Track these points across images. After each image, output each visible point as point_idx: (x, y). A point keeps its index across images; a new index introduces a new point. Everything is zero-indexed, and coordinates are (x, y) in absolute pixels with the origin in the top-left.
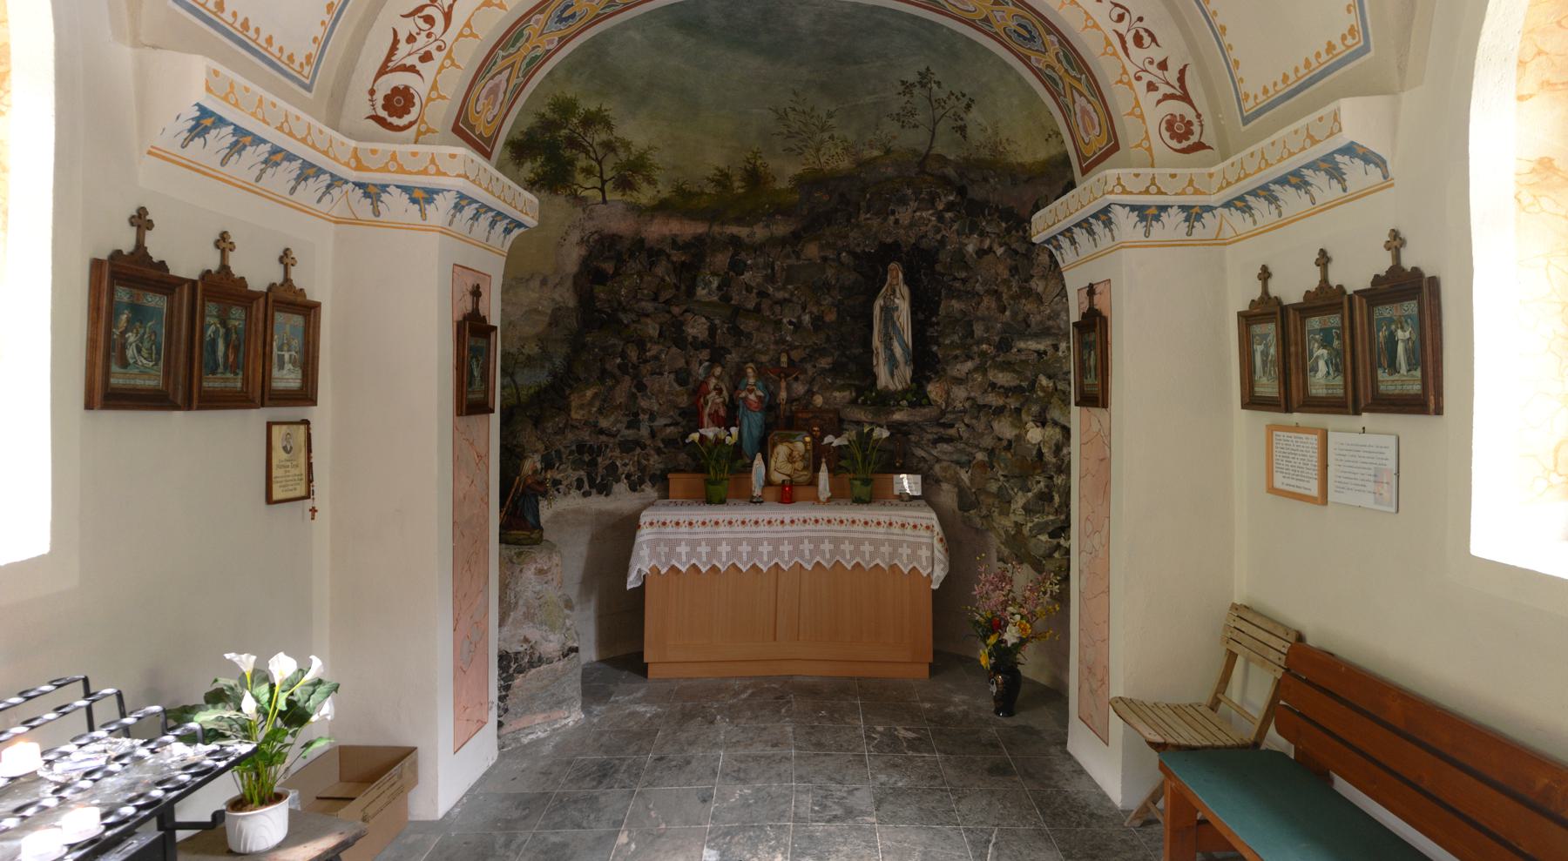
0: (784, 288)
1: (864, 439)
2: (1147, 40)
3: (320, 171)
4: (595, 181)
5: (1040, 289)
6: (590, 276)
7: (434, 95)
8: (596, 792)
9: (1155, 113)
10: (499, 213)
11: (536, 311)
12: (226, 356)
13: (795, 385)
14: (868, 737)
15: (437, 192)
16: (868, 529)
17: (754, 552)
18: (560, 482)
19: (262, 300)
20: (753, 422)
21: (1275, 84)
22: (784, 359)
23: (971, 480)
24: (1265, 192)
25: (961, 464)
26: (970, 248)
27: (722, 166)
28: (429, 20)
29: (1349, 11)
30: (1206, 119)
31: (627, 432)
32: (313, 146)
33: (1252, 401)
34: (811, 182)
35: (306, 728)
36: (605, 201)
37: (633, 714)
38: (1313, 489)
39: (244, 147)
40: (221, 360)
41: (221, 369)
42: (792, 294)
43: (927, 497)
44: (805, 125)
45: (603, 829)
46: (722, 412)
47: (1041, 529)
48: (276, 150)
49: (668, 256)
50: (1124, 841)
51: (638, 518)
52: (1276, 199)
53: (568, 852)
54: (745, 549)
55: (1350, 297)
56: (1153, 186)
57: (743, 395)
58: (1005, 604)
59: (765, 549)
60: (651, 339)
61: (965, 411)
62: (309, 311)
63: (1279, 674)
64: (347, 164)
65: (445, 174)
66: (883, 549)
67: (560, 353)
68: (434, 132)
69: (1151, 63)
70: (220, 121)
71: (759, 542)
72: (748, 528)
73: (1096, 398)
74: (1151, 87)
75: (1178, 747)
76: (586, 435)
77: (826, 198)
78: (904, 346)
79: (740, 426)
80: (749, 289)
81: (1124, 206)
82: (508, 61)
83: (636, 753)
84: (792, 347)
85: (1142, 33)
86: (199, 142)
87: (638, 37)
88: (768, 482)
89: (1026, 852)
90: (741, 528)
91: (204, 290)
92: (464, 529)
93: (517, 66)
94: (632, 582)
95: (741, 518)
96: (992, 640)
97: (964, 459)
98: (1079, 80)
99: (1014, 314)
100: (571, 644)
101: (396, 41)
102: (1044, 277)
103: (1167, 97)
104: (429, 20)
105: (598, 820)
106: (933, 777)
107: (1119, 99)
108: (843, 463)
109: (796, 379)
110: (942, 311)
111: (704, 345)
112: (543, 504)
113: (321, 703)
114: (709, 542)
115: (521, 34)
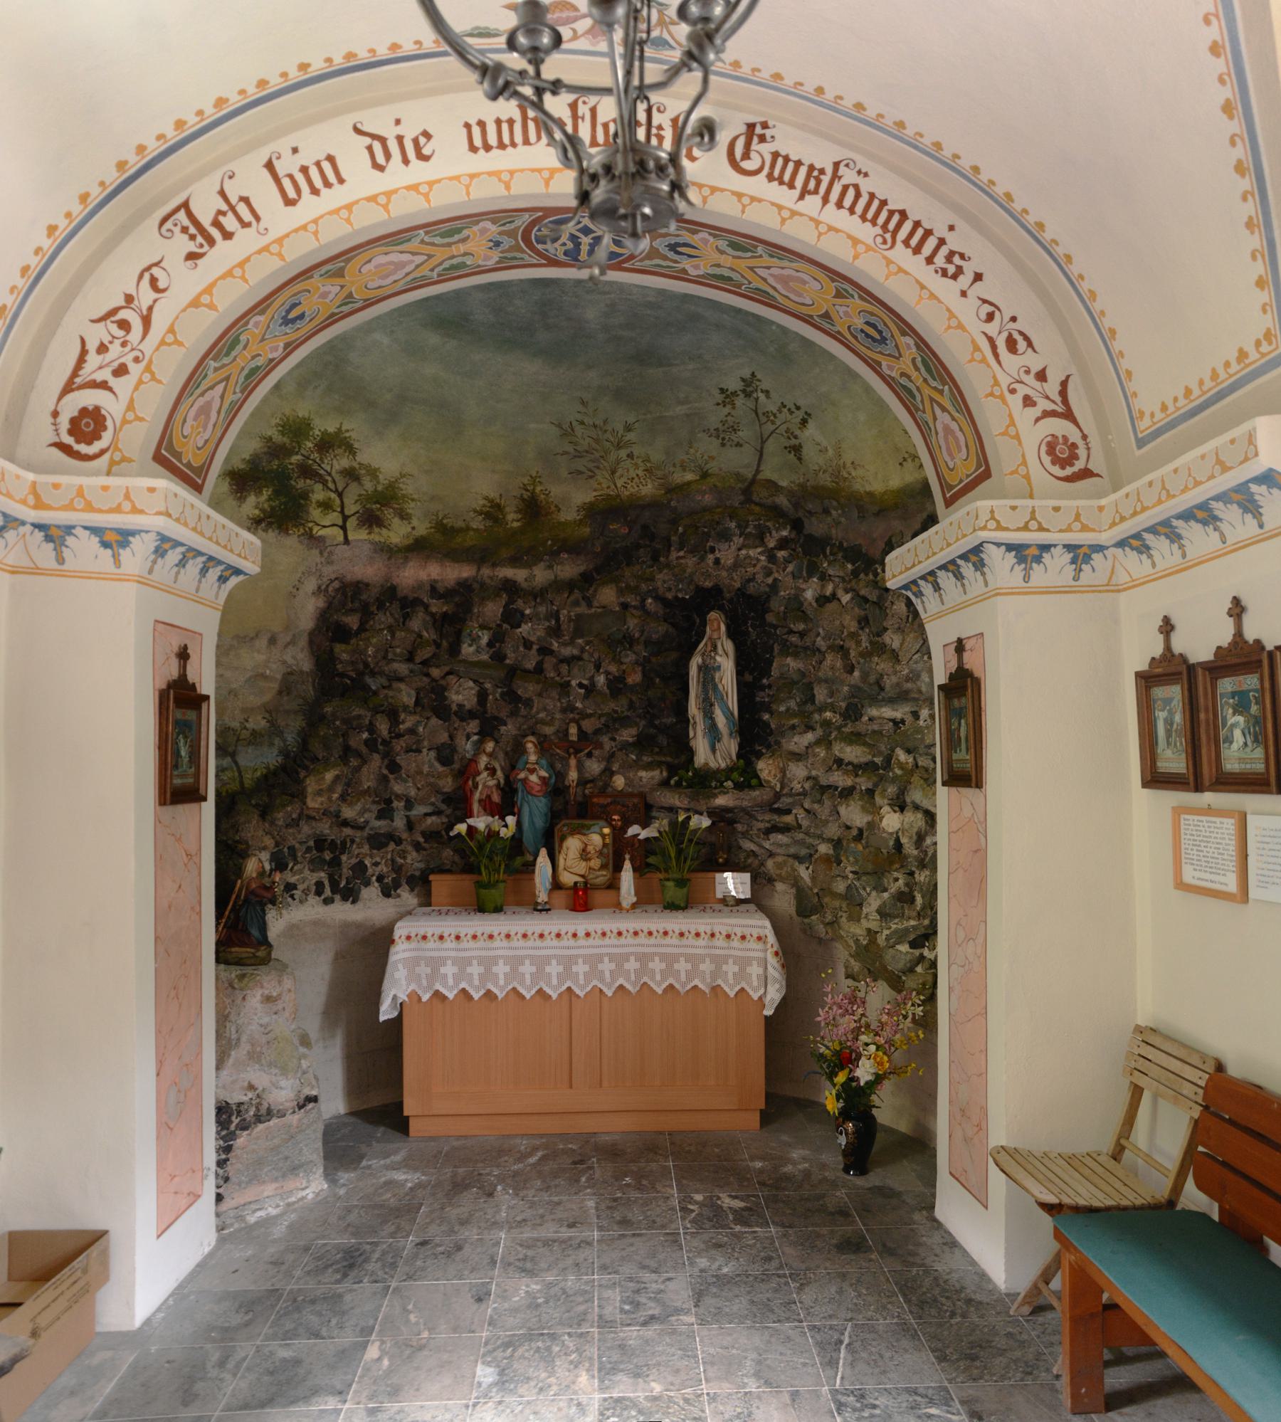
0: (572, 642)
1: (679, 830)
2: (1021, 345)
4: (335, 517)
5: (896, 645)
6: (330, 632)
7: (130, 416)
8: (340, 1288)
10: (211, 558)
11: (263, 676)
14: (683, 1209)
15: (133, 533)
16: (684, 941)
17: (539, 974)
18: (294, 887)
20: (535, 809)
21: (1176, 399)
22: (573, 730)
23: (813, 878)
24: (1165, 528)
25: (800, 859)
26: (809, 595)
27: (492, 495)
28: (124, 325)
29: (1265, 311)
30: (1094, 440)
33: (1155, 779)
34: (605, 512)
36: (346, 541)
37: (389, 1183)
38: (1230, 883)
42: (582, 650)
43: (757, 901)
44: (597, 441)
45: (347, 1338)
46: (496, 798)
47: (900, 936)
49: (426, 607)
50: (1009, 1335)
52: (1179, 537)
53: (301, 1371)
54: (527, 969)
55: (1271, 654)
56: (1032, 521)
57: (522, 775)
58: (857, 1032)
59: (554, 969)
60: (405, 708)
61: (804, 794)
63: (1196, 1112)
64: (24, 502)
65: (141, 512)
66: (702, 967)
67: (293, 727)
69: (1028, 372)
71: (547, 960)
72: (530, 943)
73: (967, 776)
74: (1028, 401)
75: (1077, 1209)
76: (325, 828)
78: (728, 713)
79: (519, 816)
80: (528, 644)
81: (998, 545)
82: (223, 374)
83: (392, 1235)
87: (386, 341)
88: (556, 885)
89: (887, 1355)
90: (522, 943)
95: (521, 930)
96: (841, 1078)
97: (804, 852)
98: (941, 392)
99: (865, 675)
101: (84, 352)
102: (900, 630)
103: (1047, 414)
104: (124, 325)
105: (341, 1327)
106: (769, 1259)
107: (990, 416)
108: (651, 860)
109: (590, 755)
110: (775, 672)
111: (472, 715)
112: (271, 915)
115: (236, 341)
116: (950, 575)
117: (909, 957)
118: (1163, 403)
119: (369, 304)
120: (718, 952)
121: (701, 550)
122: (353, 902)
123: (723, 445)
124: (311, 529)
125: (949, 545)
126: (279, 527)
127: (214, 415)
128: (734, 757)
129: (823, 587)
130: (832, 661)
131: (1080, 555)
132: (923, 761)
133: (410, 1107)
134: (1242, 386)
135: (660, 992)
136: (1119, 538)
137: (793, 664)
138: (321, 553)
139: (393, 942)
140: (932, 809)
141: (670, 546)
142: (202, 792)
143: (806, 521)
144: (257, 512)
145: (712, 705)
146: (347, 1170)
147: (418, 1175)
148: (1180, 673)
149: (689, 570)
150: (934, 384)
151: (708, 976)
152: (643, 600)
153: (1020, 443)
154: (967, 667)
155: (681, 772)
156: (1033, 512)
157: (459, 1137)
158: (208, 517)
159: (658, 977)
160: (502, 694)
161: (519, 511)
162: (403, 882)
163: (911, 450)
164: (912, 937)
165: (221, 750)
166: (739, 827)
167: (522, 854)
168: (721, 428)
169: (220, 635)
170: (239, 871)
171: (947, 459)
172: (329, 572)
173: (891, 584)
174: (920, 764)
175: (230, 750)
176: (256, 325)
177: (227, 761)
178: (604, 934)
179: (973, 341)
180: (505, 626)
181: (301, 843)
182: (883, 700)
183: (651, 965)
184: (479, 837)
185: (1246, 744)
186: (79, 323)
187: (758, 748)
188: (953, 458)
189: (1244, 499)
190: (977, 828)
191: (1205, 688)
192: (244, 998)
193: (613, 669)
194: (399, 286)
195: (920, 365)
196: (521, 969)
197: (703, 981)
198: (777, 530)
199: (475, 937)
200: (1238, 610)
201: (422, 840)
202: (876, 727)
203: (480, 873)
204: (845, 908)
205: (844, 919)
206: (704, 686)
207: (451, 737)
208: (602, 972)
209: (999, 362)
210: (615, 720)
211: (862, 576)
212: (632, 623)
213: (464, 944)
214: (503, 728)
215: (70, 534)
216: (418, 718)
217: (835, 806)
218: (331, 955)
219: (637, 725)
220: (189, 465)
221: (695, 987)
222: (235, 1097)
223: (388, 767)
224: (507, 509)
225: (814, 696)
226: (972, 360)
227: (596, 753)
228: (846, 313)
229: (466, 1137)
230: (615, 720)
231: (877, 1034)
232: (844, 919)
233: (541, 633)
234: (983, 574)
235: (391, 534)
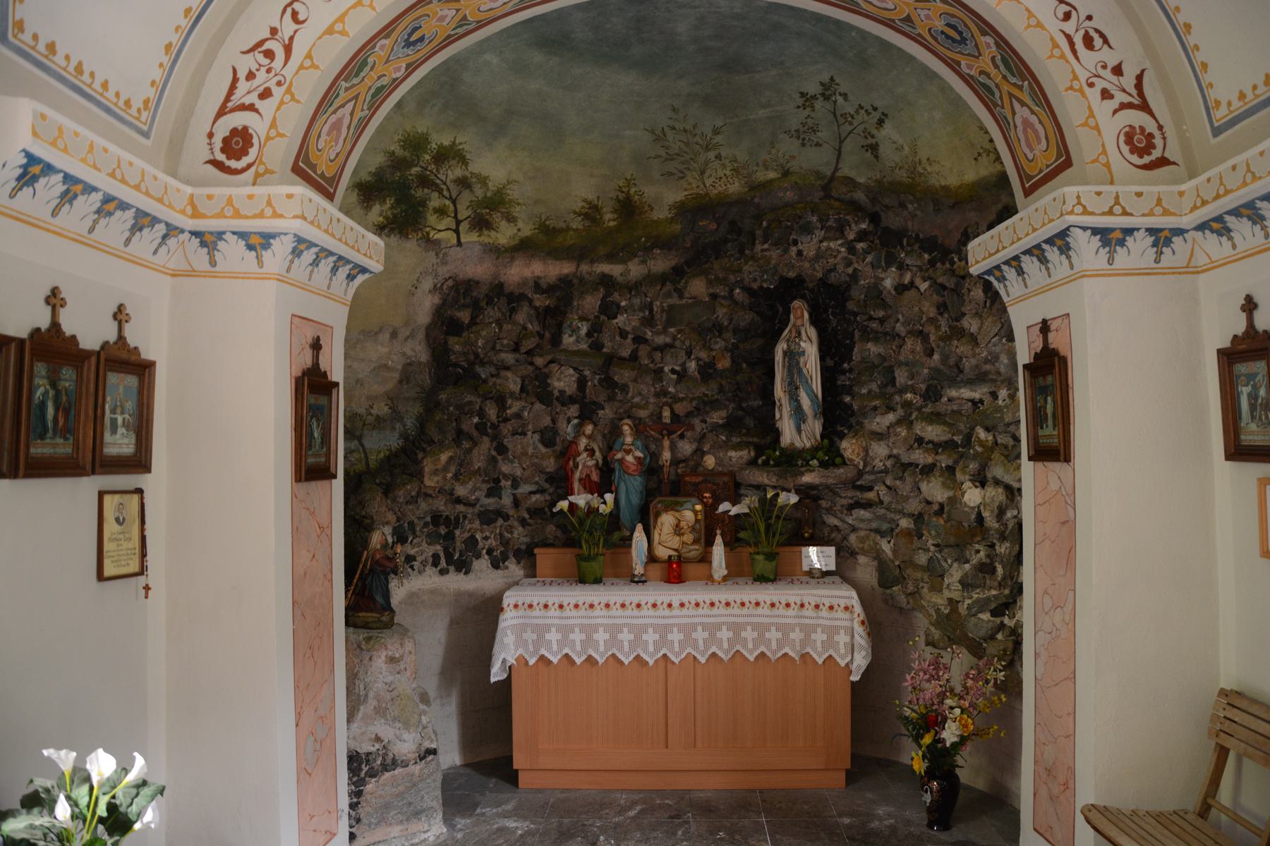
0: (665, 331)
1: (767, 506)
2: (1098, 42)
3: (155, 221)
4: (449, 222)
5: (974, 329)
6: (444, 326)
7: (273, 133)
9: (1112, 124)
10: (340, 258)
11: (386, 367)
15: (273, 236)
16: (775, 611)
19: (93, 360)
20: (631, 488)
21: (1255, 87)
22: (666, 413)
23: (894, 551)
26: (888, 283)
27: (590, 197)
28: (269, 54)
30: (1170, 131)
32: (147, 194)
33: (1237, 451)
34: (694, 210)
35: (128, 837)
36: (459, 243)
37: (502, 830)
39: (76, 196)
40: (50, 425)
41: (50, 434)
42: (674, 338)
44: (687, 144)
46: (595, 477)
47: (982, 605)
48: (108, 199)
49: (531, 301)
52: (1262, 218)
57: (619, 456)
58: (942, 696)
60: (512, 394)
61: (886, 471)
62: (143, 370)
64: (183, 212)
65: (281, 216)
66: (792, 636)
67: (411, 413)
68: (272, 172)
69: (1104, 67)
70: (49, 169)
72: (628, 612)
73: (1054, 451)
74: (1106, 94)
76: (440, 504)
78: (812, 396)
80: (623, 334)
81: (1084, 229)
82: (352, 93)
84: (676, 399)
85: (1092, 33)
86: (27, 191)
88: (652, 559)
90: (620, 612)
92: (305, 610)
93: (361, 98)
96: (927, 740)
97: (885, 526)
99: (945, 358)
102: (977, 315)
103: (1123, 106)
104: (269, 54)
107: (1070, 108)
108: (742, 535)
109: (682, 437)
110: (856, 356)
111: (572, 400)
112: (393, 583)
114: (583, 628)
115: (365, 63)
116: (1035, 259)
117: (990, 625)
118: (1241, 92)
119: (481, 25)
120: (807, 621)
121: (784, 243)
122: (466, 573)
123: (803, 145)
124: (428, 233)
125: (1034, 230)
126: (400, 233)
128: (818, 437)
129: (901, 275)
131: (1161, 238)
132: (1003, 439)
133: (519, 762)
135: (752, 659)
136: (1199, 222)
137: (873, 349)
138: (437, 255)
139: (502, 609)
140: (1016, 485)
141: (754, 240)
142: (332, 470)
143: (883, 215)
144: (381, 219)
145: (797, 388)
146: (463, 817)
147: (527, 823)
149: (773, 262)
150: (1014, 80)
151: (798, 644)
152: (732, 291)
153: (1100, 133)
154: (1052, 346)
155: (769, 452)
156: (1117, 197)
157: (564, 791)
158: (339, 220)
159: (750, 646)
160: (600, 381)
161: (615, 211)
162: (511, 555)
163: (987, 146)
164: (993, 606)
165: (348, 432)
166: (824, 503)
167: (619, 529)
168: (802, 129)
170: (365, 543)
171: (1026, 150)
172: (444, 271)
174: (999, 441)
175: (358, 433)
176: (382, 47)
177: (354, 444)
178: (697, 605)
179: (1052, 39)
180: (603, 317)
181: (419, 518)
182: (962, 381)
183: (743, 634)
184: (580, 513)
186: (233, 56)
188: (1032, 150)
190: (1068, 498)
192: (370, 659)
193: (703, 355)
195: (999, 63)
196: (620, 636)
198: (856, 223)
199: (576, 606)
201: (527, 516)
202: (955, 408)
203: (581, 547)
205: (925, 590)
207: (554, 421)
208: (696, 640)
209: (1077, 58)
210: (705, 403)
213: (567, 612)
215: (221, 239)
218: (446, 621)
219: (726, 407)
220: (322, 176)
221: (786, 655)
223: (496, 449)
225: (894, 378)
226: (1052, 56)
227: (688, 434)
228: (928, 17)
230: (705, 403)
231: (961, 698)
232: (925, 590)
233: (635, 323)
234: (1069, 257)
235: (499, 236)
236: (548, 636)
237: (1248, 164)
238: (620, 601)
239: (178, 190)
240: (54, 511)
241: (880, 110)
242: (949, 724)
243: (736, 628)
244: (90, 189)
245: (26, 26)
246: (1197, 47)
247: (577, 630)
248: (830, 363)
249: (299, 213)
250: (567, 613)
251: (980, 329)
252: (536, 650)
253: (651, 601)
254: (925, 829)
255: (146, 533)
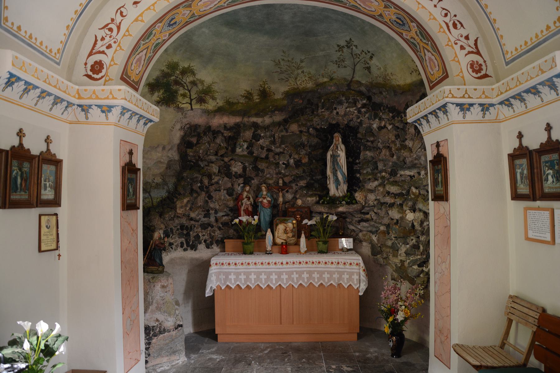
0: (280, 146)
1: (324, 221)
2: (459, 26)
3: (62, 100)
4: (187, 100)
5: (411, 145)
6: (186, 144)
9: (465, 60)
10: (141, 116)
11: (160, 162)
12: (21, 184)
13: (287, 195)
15: (112, 107)
16: (327, 266)
19: (37, 159)
20: (266, 213)
21: (521, 46)
22: (281, 182)
23: (378, 240)
24: (519, 97)
25: (373, 233)
26: (375, 126)
27: (248, 89)
28: (111, 30)
30: (488, 63)
31: (204, 219)
32: (59, 89)
33: (516, 196)
35: (53, 358)
36: (192, 109)
38: (548, 238)
39: (30, 90)
40: (19, 186)
41: (19, 190)
42: (284, 150)
44: (289, 67)
46: (250, 209)
47: (414, 262)
48: (43, 92)
49: (222, 134)
51: (210, 261)
52: (524, 100)
57: (260, 200)
58: (397, 301)
59: (274, 277)
60: (214, 174)
61: (374, 206)
62: (58, 163)
63: (535, 329)
64: (74, 97)
65: (116, 98)
66: (334, 276)
67: (171, 182)
68: (112, 80)
69: (462, 36)
70: (19, 79)
71: (271, 273)
72: (264, 266)
73: (442, 197)
74: (462, 48)
75: (487, 367)
76: (184, 221)
77: (301, 102)
78: (343, 174)
80: (262, 148)
81: (453, 104)
82: (146, 46)
84: (285, 176)
85: (456, 22)
86: (10, 88)
87: (207, 31)
88: (274, 244)
90: (261, 266)
91: (11, 155)
94: (208, 293)
96: (391, 319)
97: (374, 229)
98: (427, 44)
99: (398, 158)
100: (179, 323)
101: (96, 40)
102: (412, 139)
103: (469, 53)
104: (111, 30)
107: (448, 53)
108: (313, 233)
109: (287, 192)
110: (362, 157)
111: (240, 176)
112: (164, 255)
113: (60, 346)
114: (245, 273)
115: (151, 33)
116: (433, 116)
117: (417, 271)
119: (201, 17)
120: (340, 270)
121: (331, 109)
122: (195, 250)
123: (339, 67)
124: (178, 105)
125: (433, 104)
126: (166, 104)
127: (142, 62)
128: (346, 192)
129: (380, 123)
130: (385, 152)
132: (422, 192)
134: (548, 40)
135: (317, 286)
136: (500, 101)
137: (369, 154)
138: (182, 114)
139: (210, 265)
140: (427, 211)
141: (318, 107)
142: (138, 206)
144: (158, 99)
145: (336, 171)
146: (194, 354)
147: (221, 356)
148: (526, 154)
149: (326, 117)
152: (309, 129)
153: (460, 64)
156: (466, 91)
157: (237, 343)
159: (316, 280)
160: (252, 168)
162: (214, 242)
163: (416, 68)
164: (419, 263)
166: (348, 220)
168: (338, 60)
169: (144, 146)
170: (152, 237)
171: (430, 71)
172: (185, 121)
173: (409, 121)
179: (440, 24)
180: (253, 141)
181: (175, 227)
182: (406, 168)
183: (313, 275)
184: (244, 224)
185: (553, 181)
186: (95, 30)
187: (355, 188)
188: (433, 70)
189: (551, 84)
190: (447, 217)
191: (536, 160)
193: (296, 157)
194: (212, 10)
196: (261, 277)
197: (335, 282)
199: (242, 264)
200: (549, 128)
201: (221, 226)
202: (403, 179)
203: (244, 239)
204: (391, 252)
205: (391, 256)
206: (334, 165)
207: (232, 185)
208: (293, 278)
209: (450, 33)
210: (297, 177)
211: (396, 118)
212: (304, 138)
214: (253, 181)
215: (90, 108)
216: (219, 177)
217: (387, 211)
218: (187, 271)
219: (306, 179)
220: (133, 81)
222: (152, 324)
223: (208, 197)
224: (254, 95)
225: (377, 166)
226: (440, 32)
227: (290, 190)
228: (389, 14)
229: (240, 343)
231: (405, 301)
232: (391, 256)
234: (447, 116)
235: (209, 106)
236: (230, 277)
237: (518, 78)
238: (261, 262)
239: (72, 87)
240: (15, 225)
241: (371, 53)
242: (400, 312)
243: (310, 273)
244: (36, 87)
245: (9, 19)
246: (498, 29)
247: (242, 274)
248: (351, 160)
249: (124, 97)
250: (238, 267)
251: (413, 145)
252: (225, 282)
253: (274, 261)
254: (390, 357)
255: (59, 232)
